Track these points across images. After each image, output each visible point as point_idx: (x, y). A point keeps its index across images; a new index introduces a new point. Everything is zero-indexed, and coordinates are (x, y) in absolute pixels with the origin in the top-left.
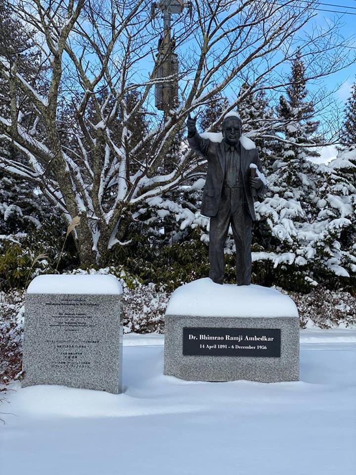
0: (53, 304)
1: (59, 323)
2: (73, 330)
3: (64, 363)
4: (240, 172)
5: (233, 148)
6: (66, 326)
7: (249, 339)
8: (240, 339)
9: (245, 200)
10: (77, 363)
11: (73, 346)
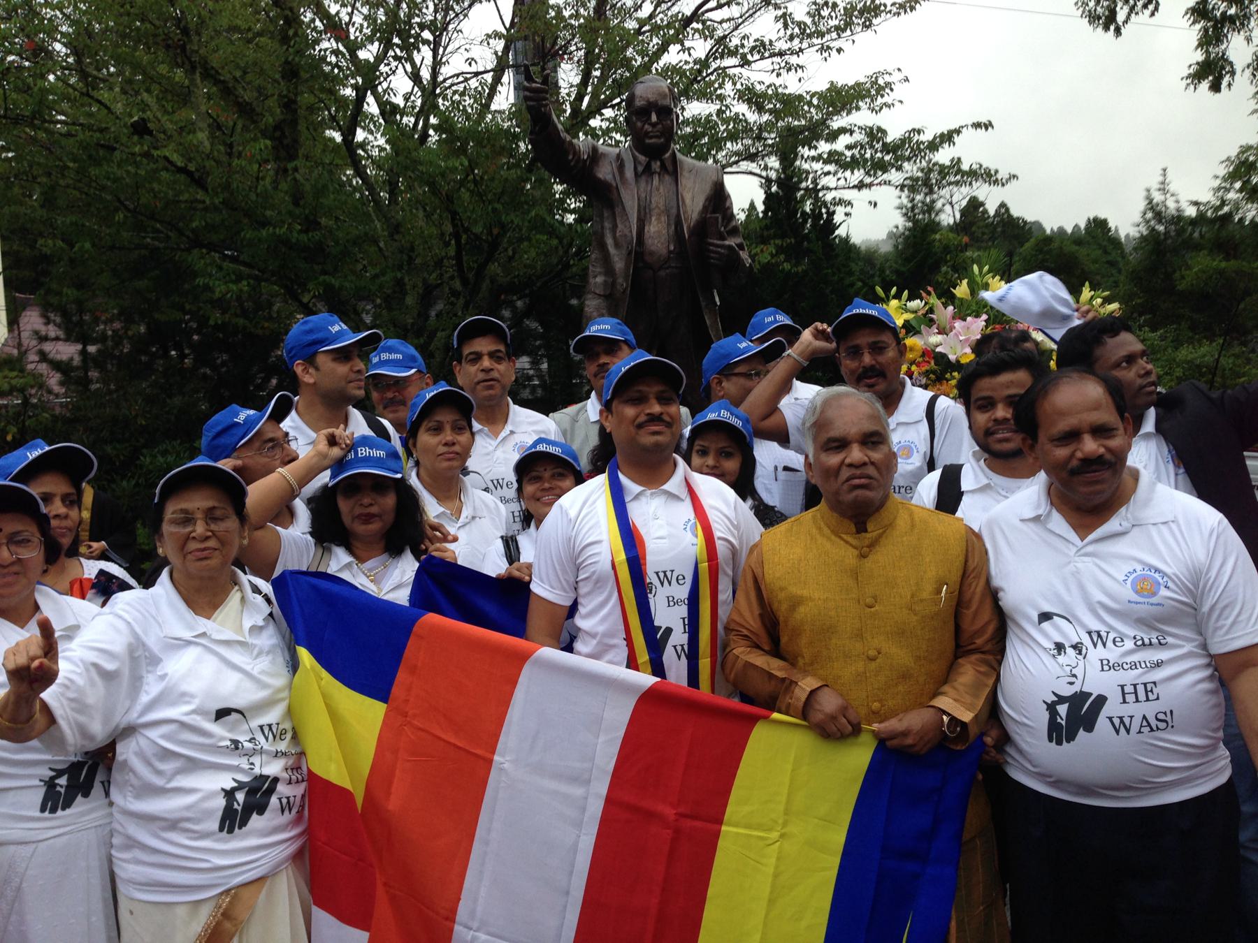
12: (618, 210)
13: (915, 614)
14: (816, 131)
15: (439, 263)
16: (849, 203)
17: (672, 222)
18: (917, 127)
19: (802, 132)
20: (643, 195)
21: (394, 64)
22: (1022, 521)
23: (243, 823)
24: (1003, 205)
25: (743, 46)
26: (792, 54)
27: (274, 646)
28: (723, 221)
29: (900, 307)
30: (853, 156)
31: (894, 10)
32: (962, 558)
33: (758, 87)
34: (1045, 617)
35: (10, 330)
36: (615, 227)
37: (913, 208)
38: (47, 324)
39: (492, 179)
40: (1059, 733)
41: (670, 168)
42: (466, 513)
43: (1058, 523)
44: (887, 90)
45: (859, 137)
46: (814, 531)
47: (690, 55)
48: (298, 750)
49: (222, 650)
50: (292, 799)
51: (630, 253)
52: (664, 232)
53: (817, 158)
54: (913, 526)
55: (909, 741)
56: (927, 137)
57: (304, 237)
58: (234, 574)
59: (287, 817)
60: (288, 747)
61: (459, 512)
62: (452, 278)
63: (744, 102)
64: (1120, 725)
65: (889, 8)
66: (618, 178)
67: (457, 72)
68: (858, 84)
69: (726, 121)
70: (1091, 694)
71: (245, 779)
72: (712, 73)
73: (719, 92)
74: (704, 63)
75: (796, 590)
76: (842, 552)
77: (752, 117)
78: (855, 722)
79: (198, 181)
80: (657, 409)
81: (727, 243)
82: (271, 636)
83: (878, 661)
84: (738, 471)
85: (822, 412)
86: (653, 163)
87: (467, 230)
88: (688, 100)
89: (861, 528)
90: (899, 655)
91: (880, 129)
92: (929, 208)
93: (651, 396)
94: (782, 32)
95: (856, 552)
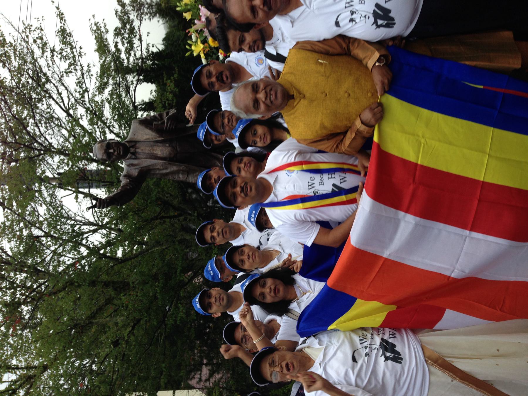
12: (151, 168)
13: (331, 75)
14: (116, 58)
16: (148, 45)
17: (157, 144)
18: (114, 12)
19: (117, 64)
20: (145, 156)
21: (89, 243)
22: (293, 27)
23: (399, 354)
25: (79, 92)
26: (83, 69)
27: (328, 336)
29: (195, 45)
30: (127, 43)
31: (63, 22)
32: (307, 52)
33: (97, 85)
34: (337, 24)
36: (158, 169)
37: (150, 13)
38: (194, 378)
39: (138, 204)
40: (390, 23)
41: (133, 144)
42: (278, 248)
43: (295, 13)
44: (98, 25)
45: (119, 40)
46: (292, 116)
47: (83, 116)
48: (371, 329)
49: (328, 358)
50: (391, 333)
51: (170, 164)
52: (161, 148)
53: (128, 59)
54: (292, 73)
55: (386, 81)
56: (119, 8)
57: (161, 281)
58: (298, 351)
59: (397, 335)
60: (369, 333)
61: (277, 251)
62: (179, 220)
63: (104, 91)
65: (62, 25)
66: (137, 167)
67: (92, 215)
68: (96, 38)
69: (112, 99)
70: (374, 10)
71: (381, 352)
72: (92, 106)
73: (100, 103)
74: (87, 109)
75: (318, 126)
76: (302, 105)
77: (110, 88)
78: (377, 105)
79: (137, 322)
80: (238, 189)
81: (166, 121)
82: (324, 337)
83: (350, 93)
84: (264, 127)
85: (241, 109)
87: (160, 213)
88: (103, 117)
89: (292, 97)
90: (348, 83)
91: (116, 30)
93: (233, 190)
94: (73, 74)
95: (302, 100)
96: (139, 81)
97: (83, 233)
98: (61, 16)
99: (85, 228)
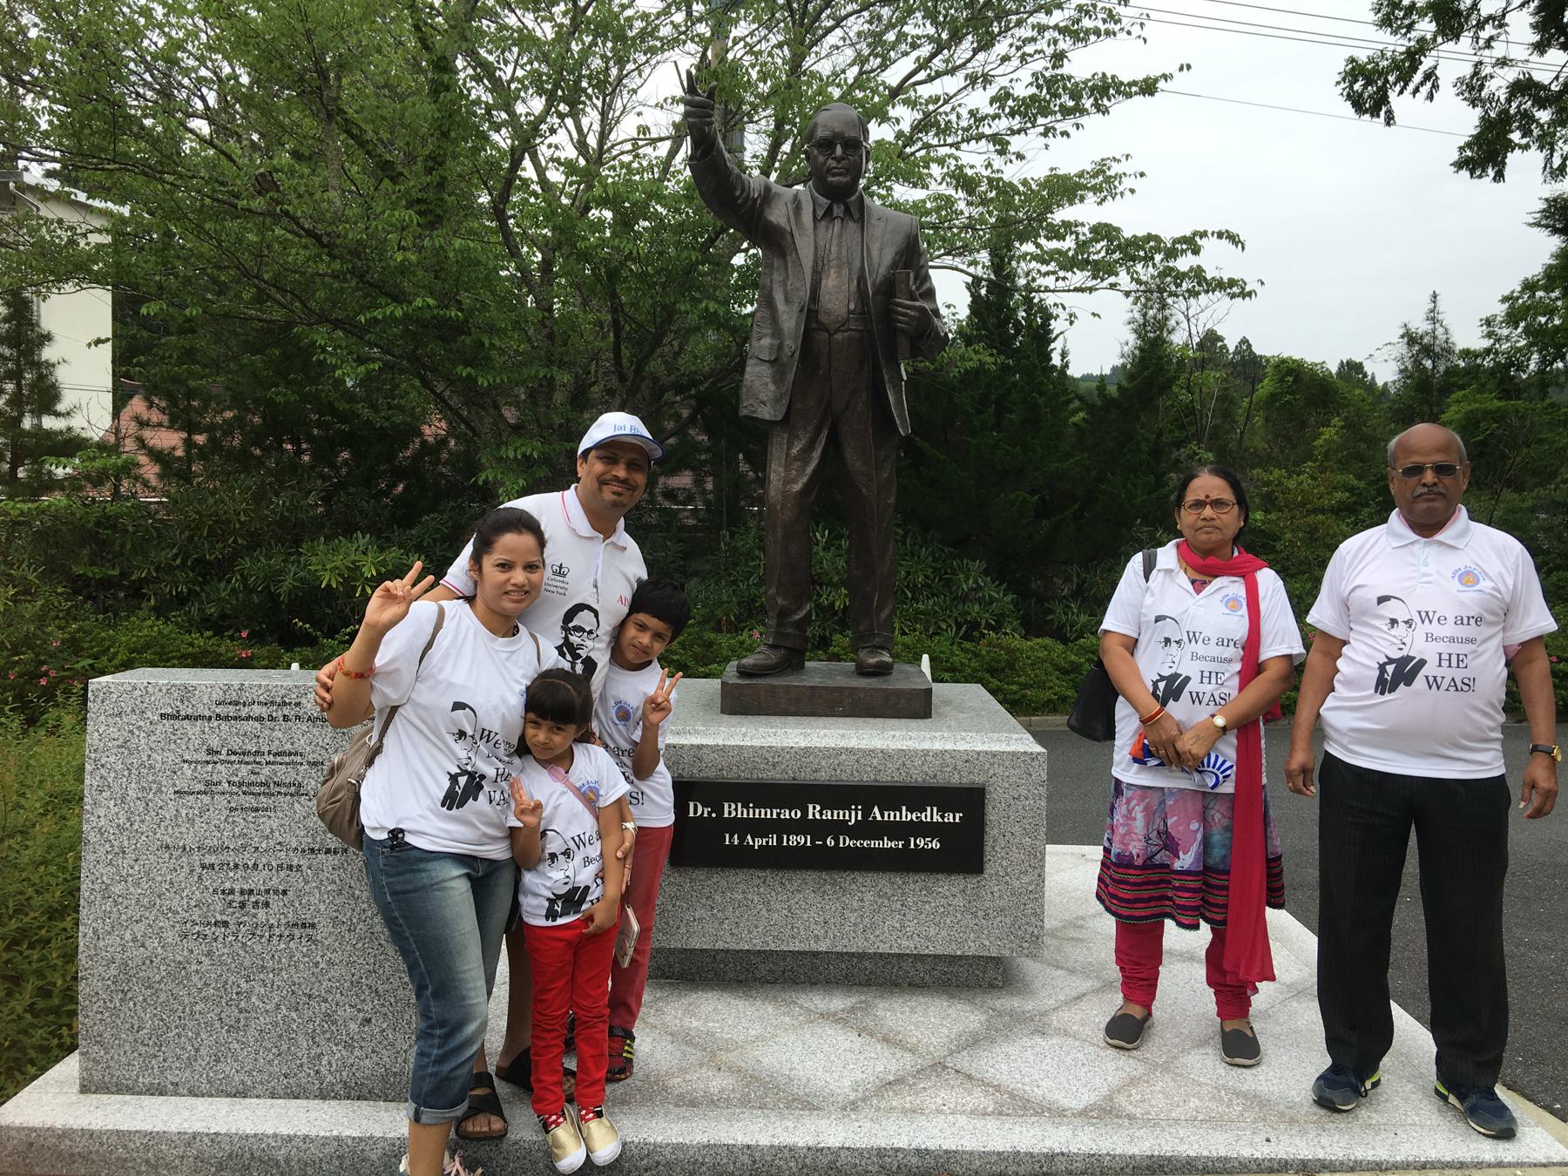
0: (187, 717)
1: (208, 783)
2: (257, 810)
3: (226, 924)
4: (861, 279)
5: (838, 210)
6: (232, 794)
7: (883, 816)
8: (853, 816)
9: (876, 370)
10: (271, 927)
11: (255, 866)
15: (595, 357)
24: (1244, 341)
28: (916, 279)
35: (113, 420)
38: (150, 407)
41: (856, 215)
64: (1433, 683)
66: (793, 222)
86: (835, 207)
92: (1161, 324)
96: (977, 280)
97: (575, 114)
98: (1148, 87)
99: (591, 119)
